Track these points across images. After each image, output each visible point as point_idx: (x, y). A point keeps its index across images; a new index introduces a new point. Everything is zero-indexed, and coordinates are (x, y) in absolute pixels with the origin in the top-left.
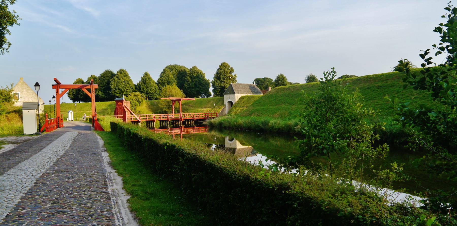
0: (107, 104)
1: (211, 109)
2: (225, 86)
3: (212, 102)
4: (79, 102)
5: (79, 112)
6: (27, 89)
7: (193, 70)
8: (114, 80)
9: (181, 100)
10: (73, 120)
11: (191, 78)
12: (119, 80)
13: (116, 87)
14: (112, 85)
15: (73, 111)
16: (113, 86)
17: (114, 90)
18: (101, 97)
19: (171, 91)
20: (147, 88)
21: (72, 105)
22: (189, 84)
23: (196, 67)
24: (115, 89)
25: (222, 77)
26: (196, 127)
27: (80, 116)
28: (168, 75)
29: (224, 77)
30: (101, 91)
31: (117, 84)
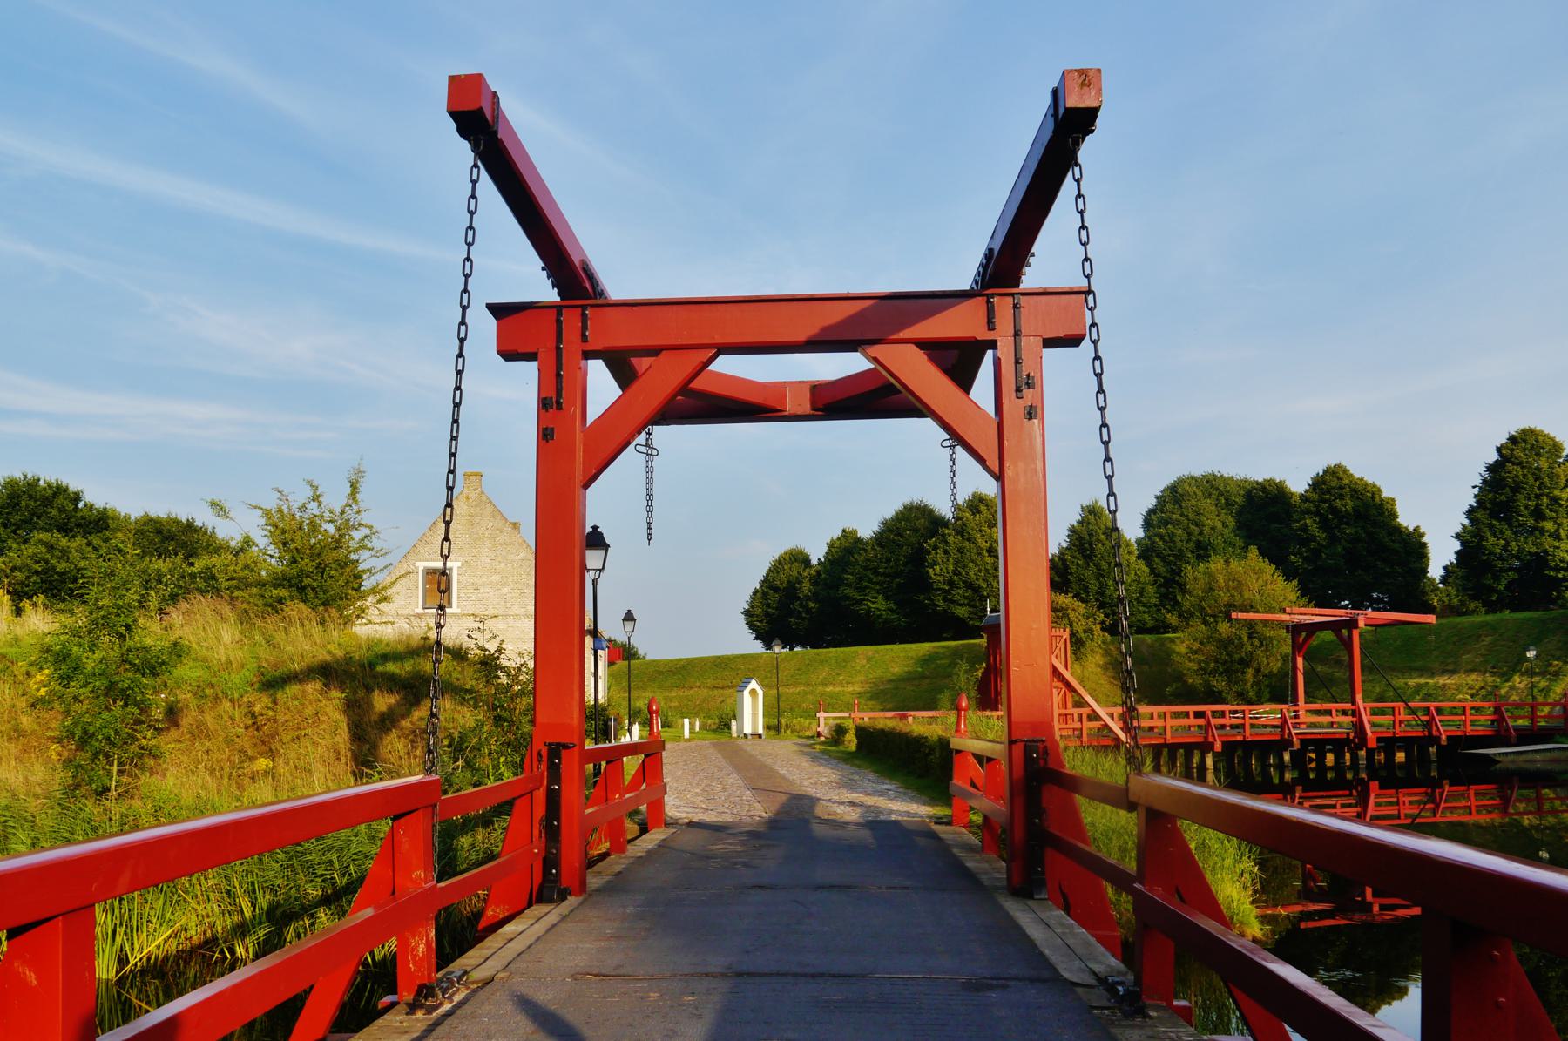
0: (912, 654)
1: (1489, 679)
2: (1546, 552)
3: (1488, 640)
4: (791, 649)
5: (792, 690)
6: (501, 538)
7: (1334, 484)
8: (947, 543)
9: (1361, 624)
10: (761, 731)
11: (1324, 524)
12: (967, 544)
13: (956, 572)
14: (938, 568)
15: (763, 686)
16: (939, 571)
17: (948, 592)
18: (886, 621)
19: (1240, 587)
20: (1100, 575)
21: (762, 661)
22: (1316, 553)
23: (1345, 471)
24: (951, 583)
25: (1527, 507)
26: (1450, 785)
27: (792, 709)
28: (1198, 514)
29: (1537, 507)
30: (887, 598)
31: (957, 562)
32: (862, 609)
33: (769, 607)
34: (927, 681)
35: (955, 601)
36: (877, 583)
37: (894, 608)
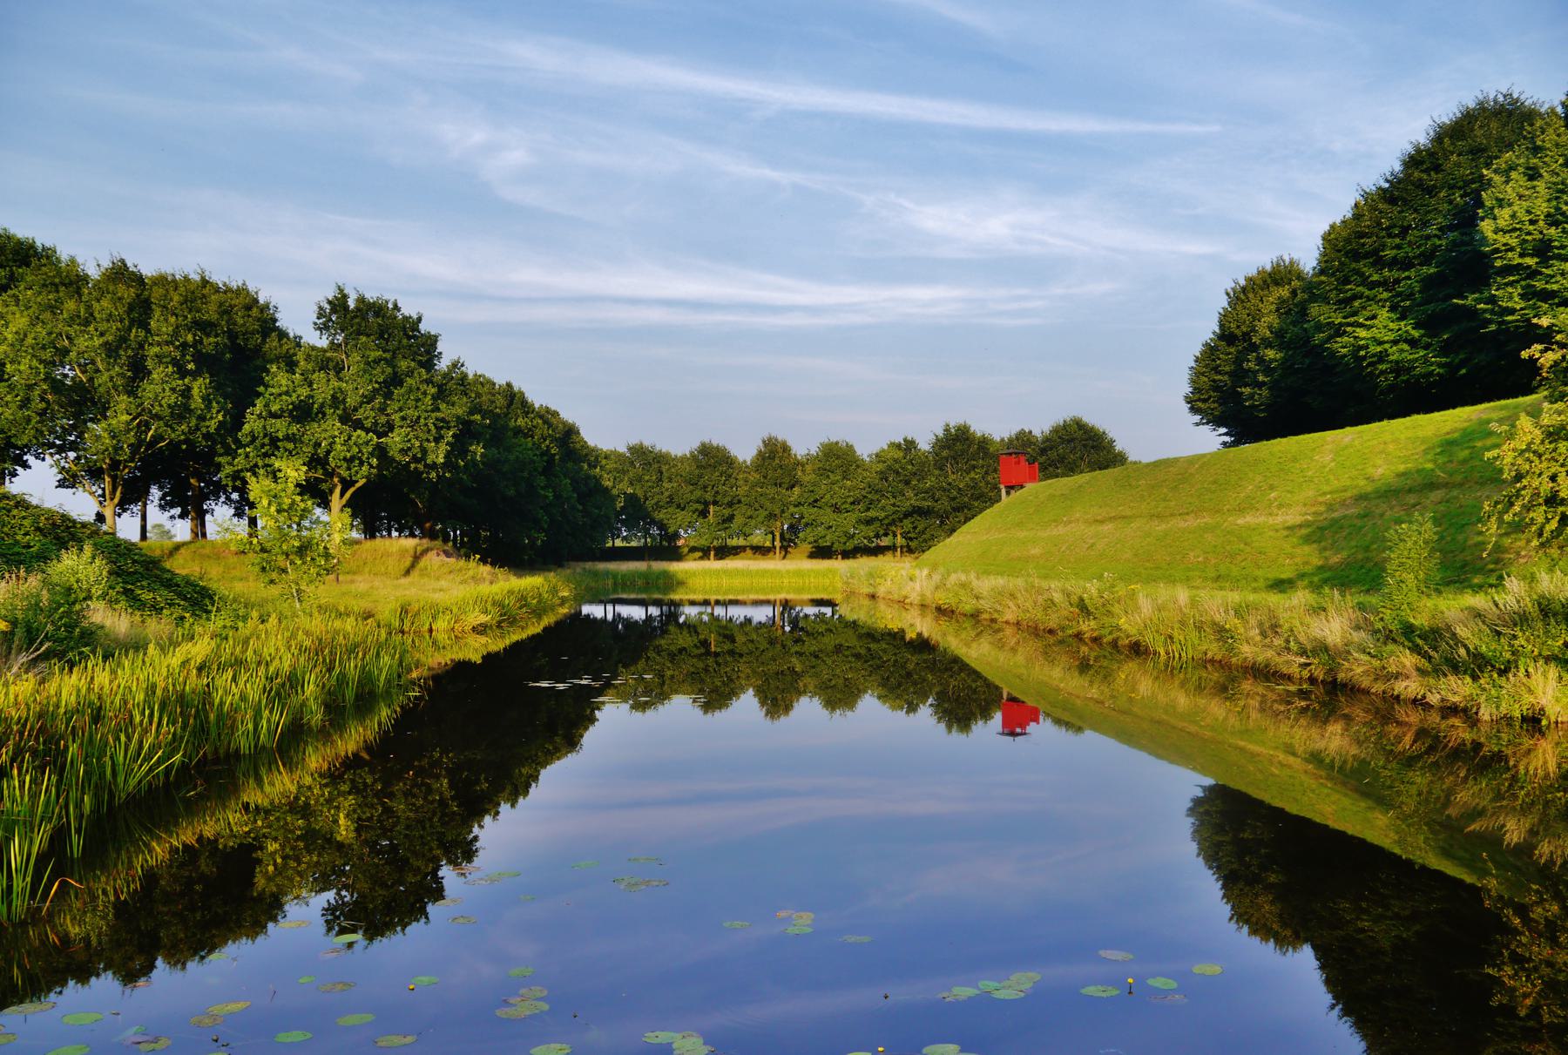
18: (1398, 368)
32: (1341, 346)
33: (1219, 373)
34: (1437, 495)
35: (1553, 294)
36: (1383, 284)
37: (1416, 334)
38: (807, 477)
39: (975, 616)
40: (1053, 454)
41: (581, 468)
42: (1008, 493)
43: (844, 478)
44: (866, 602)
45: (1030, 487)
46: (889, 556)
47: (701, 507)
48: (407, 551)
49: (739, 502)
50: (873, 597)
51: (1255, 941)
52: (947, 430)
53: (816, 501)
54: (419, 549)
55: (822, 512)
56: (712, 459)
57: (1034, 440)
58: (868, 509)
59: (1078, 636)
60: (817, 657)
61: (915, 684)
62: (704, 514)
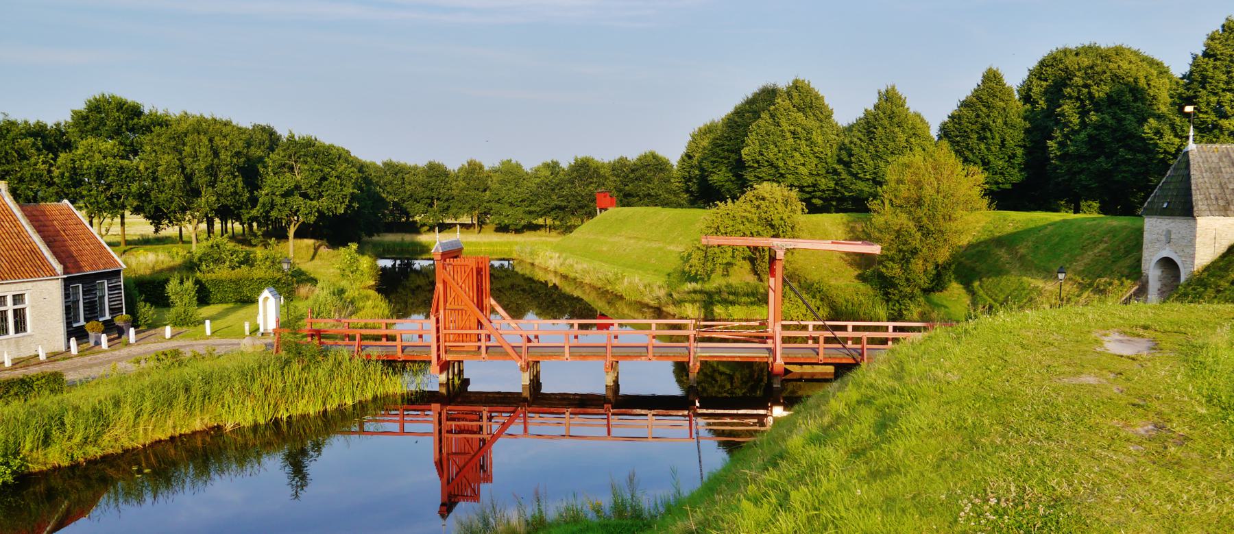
38: (494, 185)
39: (575, 279)
40: (638, 174)
41: (371, 189)
42: (601, 212)
43: (516, 186)
44: (529, 266)
45: (611, 209)
46: (542, 232)
47: (429, 201)
48: (310, 246)
49: (453, 198)
50: (533, 264)
51: (222, 115)
52: (576, 160)
53: (500, 199)
54: (317, 244)
55: (503, 206)
56: (436, 172)
57: (627, 163)
58: (530, 205)
59: (607, 291)
60: (500, 291)
61: (557, 306)
62: (431, 205)
